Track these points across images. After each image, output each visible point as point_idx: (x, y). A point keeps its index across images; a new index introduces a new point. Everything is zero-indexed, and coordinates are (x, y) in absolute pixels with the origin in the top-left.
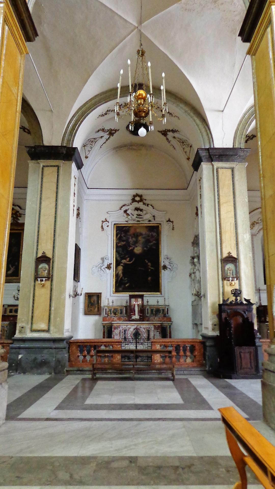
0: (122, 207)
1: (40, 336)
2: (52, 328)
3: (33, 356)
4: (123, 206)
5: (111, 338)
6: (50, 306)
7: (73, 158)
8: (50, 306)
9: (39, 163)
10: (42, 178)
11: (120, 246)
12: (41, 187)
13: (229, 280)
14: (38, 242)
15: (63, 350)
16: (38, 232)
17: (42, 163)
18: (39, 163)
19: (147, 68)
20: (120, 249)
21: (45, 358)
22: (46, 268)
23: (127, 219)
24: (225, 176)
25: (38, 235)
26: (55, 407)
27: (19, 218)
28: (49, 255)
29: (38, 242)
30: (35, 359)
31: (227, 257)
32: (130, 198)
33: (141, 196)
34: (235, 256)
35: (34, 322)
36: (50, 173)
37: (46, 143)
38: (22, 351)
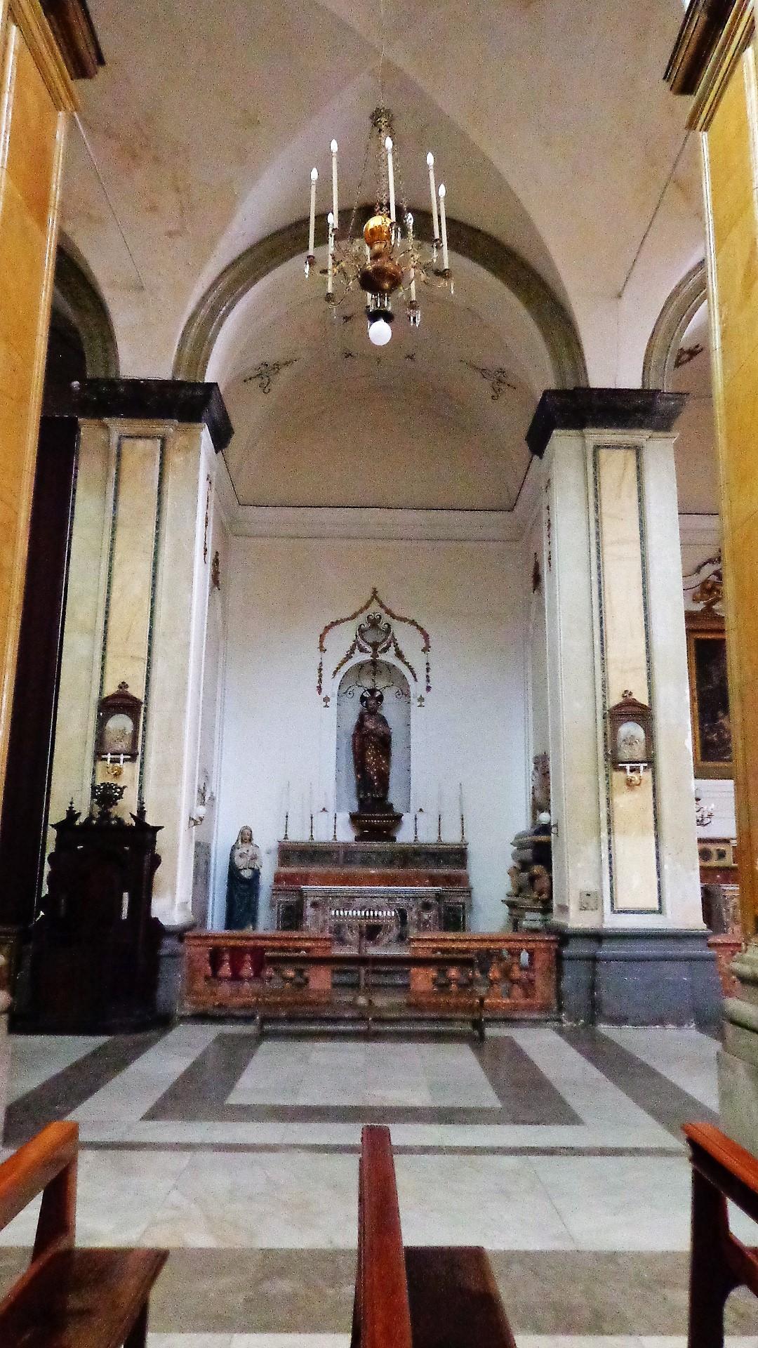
7: (205, 415)
9: (105, 427)
10: (639, 478)
13: (624, 769)
17: (594, 436)
18: (105, 427)
24: (616, 466)
26: (145, 1108)
28: (137, 691)
31: (114, 697)
34: (647, 704)
36: (616, 466)
37: (599, 378)
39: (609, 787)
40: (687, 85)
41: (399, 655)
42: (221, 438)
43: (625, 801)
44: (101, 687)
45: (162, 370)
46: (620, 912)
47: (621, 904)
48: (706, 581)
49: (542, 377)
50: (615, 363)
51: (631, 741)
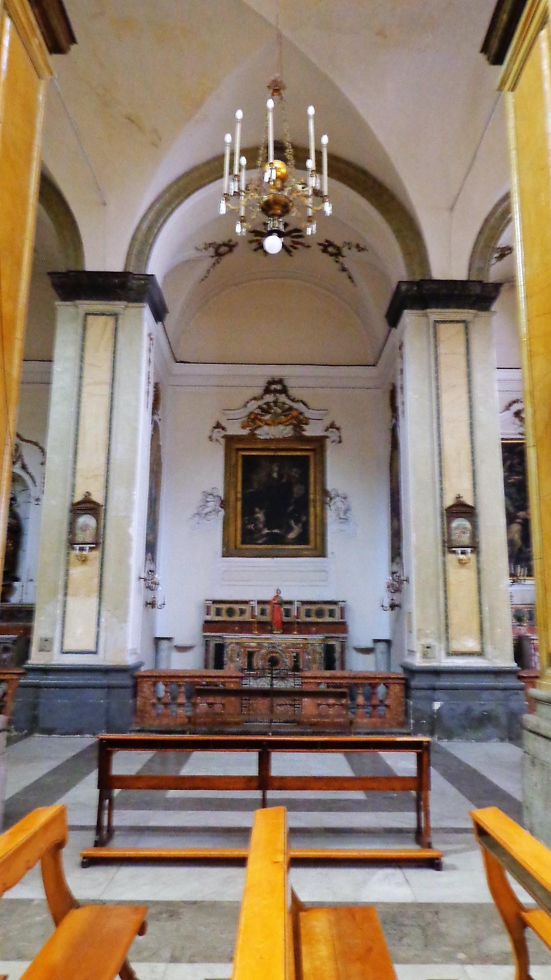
0: (510, 405)
1: (467, 665)
2: (489, 649)
3: (461, 708)
4: (514, 402)
5: (222, 668)
6: (480, 604)
8: (480, 604)
9: (76, 306)
11: (513, 484)
12: (437, 365)
13: (454, 552)
14: (441, 475)
15: (520, 692)
16: (440, 454)
17: (435, 314)
19: (306, 117)
20: (513, 490)
21: (486, 708)
22: (465, 528)
23: (521, 430)
25: (440, 461)
27: (305, 427)
28: (97, 497)
29: (441, 475)
30: (468, 711)
32: (263, 383)
33: (280, 382)
35: (450, 636)
36: (451, 336)
37: (438, 273)
38: (439, 694)
39: (68, 563)
40: (498, 59)
41: (24, 467)
42: (159, 314)
43: (78, 572)
44: (442, 497)
45: (115, 263)
46: (67, 653)
47: (67, 647)
48: (252, 413)
49: (399, 271)
50: (448, 262)
51: (85, 528)
